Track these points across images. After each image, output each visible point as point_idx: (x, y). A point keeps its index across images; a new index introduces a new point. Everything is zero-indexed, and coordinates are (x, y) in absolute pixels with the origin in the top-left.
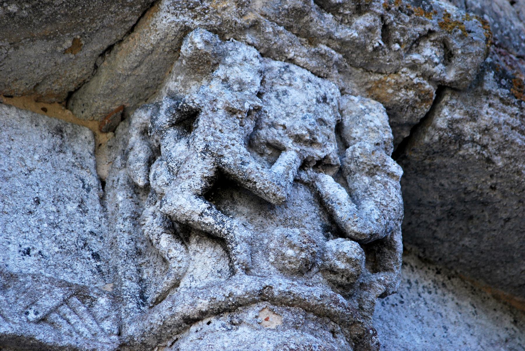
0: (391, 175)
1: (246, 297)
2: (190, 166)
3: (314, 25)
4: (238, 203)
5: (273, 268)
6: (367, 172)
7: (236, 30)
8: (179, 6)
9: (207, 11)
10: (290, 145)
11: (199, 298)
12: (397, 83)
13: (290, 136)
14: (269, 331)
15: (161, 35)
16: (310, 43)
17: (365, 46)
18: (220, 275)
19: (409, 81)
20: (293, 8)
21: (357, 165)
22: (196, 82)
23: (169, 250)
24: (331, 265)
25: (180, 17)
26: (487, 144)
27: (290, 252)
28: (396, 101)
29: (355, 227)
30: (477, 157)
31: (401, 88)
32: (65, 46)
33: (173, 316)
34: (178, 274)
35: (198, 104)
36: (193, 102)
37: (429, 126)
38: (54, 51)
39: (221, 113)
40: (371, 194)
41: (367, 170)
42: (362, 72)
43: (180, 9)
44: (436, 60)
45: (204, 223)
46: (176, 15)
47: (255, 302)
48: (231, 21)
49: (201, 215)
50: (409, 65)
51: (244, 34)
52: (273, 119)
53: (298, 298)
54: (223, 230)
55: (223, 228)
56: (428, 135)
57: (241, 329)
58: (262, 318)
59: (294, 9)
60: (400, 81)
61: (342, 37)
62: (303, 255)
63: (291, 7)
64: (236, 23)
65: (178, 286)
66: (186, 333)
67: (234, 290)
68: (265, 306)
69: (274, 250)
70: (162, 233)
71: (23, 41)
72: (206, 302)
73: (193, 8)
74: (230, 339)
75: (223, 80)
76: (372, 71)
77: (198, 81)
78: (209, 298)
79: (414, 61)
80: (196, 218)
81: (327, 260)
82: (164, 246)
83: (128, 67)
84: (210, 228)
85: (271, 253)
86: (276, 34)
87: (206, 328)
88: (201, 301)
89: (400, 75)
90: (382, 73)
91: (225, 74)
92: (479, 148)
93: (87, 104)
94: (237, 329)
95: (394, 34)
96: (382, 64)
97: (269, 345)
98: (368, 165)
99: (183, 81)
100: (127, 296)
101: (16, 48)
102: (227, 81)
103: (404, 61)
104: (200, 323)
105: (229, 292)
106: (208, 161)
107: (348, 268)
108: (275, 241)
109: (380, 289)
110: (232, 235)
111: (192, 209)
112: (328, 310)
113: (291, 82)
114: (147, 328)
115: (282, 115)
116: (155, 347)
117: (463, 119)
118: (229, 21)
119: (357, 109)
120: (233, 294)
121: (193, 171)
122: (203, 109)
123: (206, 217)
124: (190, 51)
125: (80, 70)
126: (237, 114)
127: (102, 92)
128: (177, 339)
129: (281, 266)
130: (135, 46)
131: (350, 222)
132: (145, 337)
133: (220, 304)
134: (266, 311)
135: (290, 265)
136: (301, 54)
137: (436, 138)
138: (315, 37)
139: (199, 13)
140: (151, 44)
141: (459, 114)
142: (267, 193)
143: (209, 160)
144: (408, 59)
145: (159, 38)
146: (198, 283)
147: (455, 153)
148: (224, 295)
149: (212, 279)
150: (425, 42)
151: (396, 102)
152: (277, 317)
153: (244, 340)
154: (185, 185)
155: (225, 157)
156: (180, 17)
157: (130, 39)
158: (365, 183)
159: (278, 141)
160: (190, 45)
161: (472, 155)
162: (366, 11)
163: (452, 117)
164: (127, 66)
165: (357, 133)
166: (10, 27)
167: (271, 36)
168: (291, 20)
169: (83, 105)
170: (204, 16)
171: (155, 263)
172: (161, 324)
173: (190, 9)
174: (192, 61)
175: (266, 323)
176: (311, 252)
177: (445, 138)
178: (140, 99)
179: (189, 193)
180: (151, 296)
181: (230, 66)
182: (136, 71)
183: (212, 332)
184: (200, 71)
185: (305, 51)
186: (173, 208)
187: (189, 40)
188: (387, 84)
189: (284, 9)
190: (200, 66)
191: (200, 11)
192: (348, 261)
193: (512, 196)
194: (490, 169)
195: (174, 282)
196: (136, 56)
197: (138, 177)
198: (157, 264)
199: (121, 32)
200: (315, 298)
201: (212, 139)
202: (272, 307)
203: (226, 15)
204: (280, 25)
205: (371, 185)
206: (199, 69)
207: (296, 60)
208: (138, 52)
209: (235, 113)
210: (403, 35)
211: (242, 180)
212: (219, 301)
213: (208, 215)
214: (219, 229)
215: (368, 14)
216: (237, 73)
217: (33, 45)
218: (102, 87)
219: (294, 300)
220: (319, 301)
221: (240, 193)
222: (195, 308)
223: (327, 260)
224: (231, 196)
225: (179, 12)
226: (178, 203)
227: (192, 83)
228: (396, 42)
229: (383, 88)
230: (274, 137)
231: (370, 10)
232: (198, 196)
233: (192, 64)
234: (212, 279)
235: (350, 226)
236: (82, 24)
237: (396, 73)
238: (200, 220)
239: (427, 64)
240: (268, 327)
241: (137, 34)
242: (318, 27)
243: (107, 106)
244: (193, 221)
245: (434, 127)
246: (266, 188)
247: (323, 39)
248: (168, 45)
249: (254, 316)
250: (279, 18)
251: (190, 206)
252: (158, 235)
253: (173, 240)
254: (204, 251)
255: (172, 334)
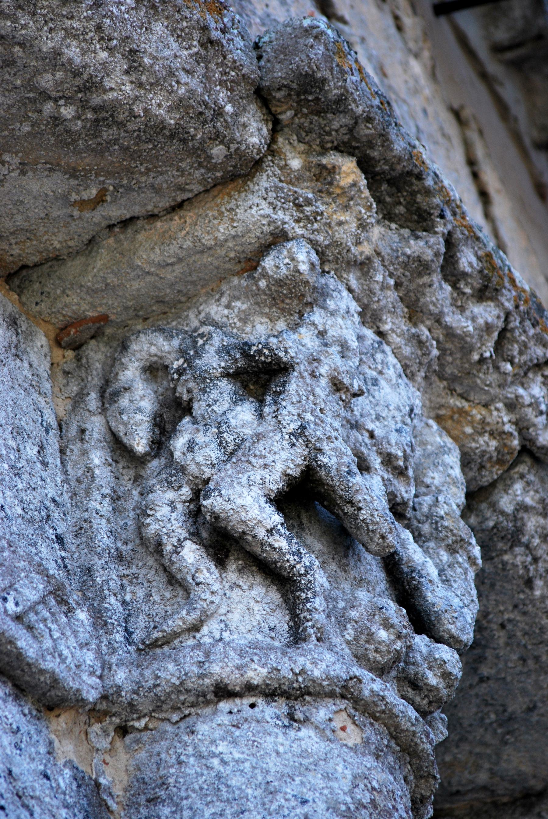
0: (471, 560)
1: (325, 683)
2: (268, 449)
3: (430, 292)
4: (307, 531)
5: (347, 651)
6: (448, 545)
7: (342, 262)
8: (283, 195)
9: (319, 218)
10: (378, 466)
11: (253, 661)
12: (483, 421)
13: (380, 453)
14: (345, 749)
15: (239, 229)
16: (410, 319)
17: (471, 350)
18: (273, 634)
19: (500, 425)
20: (419, 257)
21: (436, 529)
22: (267, 320)
23: (197, 570)
24: (417, 673)
25: (280, 212)
26: (540, 558)
27: (383, 634)
28: (471, 448)
29: (453, 626)
30: (521, 572)
31: (486, 432)
32: (85, 196)
33: (201, 676)
34: (205, 612)
35: (292, 358)
36: (286, 352)
37: (482, 502)
38: (65, 197)
39: (324, 382)
40: (448, 581)
41: (450, 542)
42: (444, 388)
43: (283, 200)
44: (543, 407)
45: (270, 545)
46: (274, 208)
47: (332, 695)
48: (344, 245)
49: (270, 531)
50: (507, 401)
51: (349, 272)
52: (359, 417)
53: (391, 710)
54: (298, 566)
55: (300, 563)
56: (477, 516)
57: (305, 732)
58: (337, 724)
59: (419, 259)
60: (488, 420)
61: (454, 325)
62: (398, 645)
63: (416, 255)
64: (349, 251)
65: (198, 630)
66: (208, 710)
67: (309, 666)
68: (343, 707)
69: (356, 622)
70: (185, 539)
71: (39, 166)
72: (264, 671)
73: (301, 206)
74: (288, 743)
75: (319, 332)
76: (455, 391)
77: (271, 320)
78: (269, 666)
79: (517, 397)
80: (261, 533)
81: (413, 664)
82: (190, 561)
83: (156, 260)
84: (276, 557)
85: (349, 626)
86: (384, 287)
87: (248, 712)
88: (256, 667)
89: (490, 411)
90: (467, 400)
91: (324, 324)
92: (529, 559)
93: (49, 293)
94: (299, 729)
95: (510, 347)
96: (477, 385)
97: (346, 772)
98: (454, 535)
99: (244, 311)
100: (113, 621)
101: (23, 173)
102: (323, 336)
103: (504, 392)
104: (238, 701)
105: (301, 668)
106: (299, 451)
107: (440, 686)
108: (362, 609)
109: (442, 733)
110: (312, 579)
111: (259, 518)
112: (416, 744)
113: (383, 368)
114: (146, 681)
115: (371, 414)
116: (144, 716)
117: (534, 508)
118: (341, 244)
119: (435, 442)
120: (305, 673)
121: (272, 459)
122: (297, 367)
123: (277, 537)
124: (285, 271)
125: (68, 238)
126: (342, 392)
127: (89, 284)
128: (190, 714)
129: (360, 651)
130: (184, 232)
131: (447, 616)
132: (138, 695)
133: (282, 681)
134: (344, 714)
135: (375, 654)
136: (398, 331)
137: (491, 524)
138: (422, 312)
139: (307, 216)
140: (216, 239)
141: (532, 499)
142: (373, 531)
143: (300, 450)
144: (511, 392)
145: (233, 232)
146: (235, 637)
147: (497, 556)
148: (292, 670)
149: (259, 637)
150: (535, 373)
151: (469, 450)
152: (357, 730)
153: (310, 750)
154: (257, 475)
155: (324, 454)
156: (279, 212)
157: (176, 218)
158: (441, 561)
159: (363, 454)
160: (287, 261)
161: (517, 566)
162: (491, 299)
163: (523, 501)
164: (156, 256)
165: (433, 478)
166: (41, 139)
167: (377, 287)
168: (407, 273)
169: (42, 293)
170: (312, 224)
171: (150, 582)
172: (178, 683)
173: (296, 205)
174: (281, 286)
175: (341, 734)
176: (408, 644)
177: (503, 527)
178: (136, 315)
179: (259, 492)
180: (138, 631)
181: (333, 314)
182: (164, 271)
183: (258, 721)
184: (282, 305)
185: (405, 328)
186: (230, 507)
187: (285, 252)
188: (469, 418)
189: (404, 254)
190: (287, 298)
191: (309, 214)
192: (443, 675)
193: (519, 645)
194: (522, 596)
195: (194, 622)
196: (181, 247)
197: (137, 438)
198: (154, 584)
199: (165, 203)
200: (410, 720)
201: (312, 419)
202: (352, 711)
203: (341, 234)
204: (391, 275)
205: (449, 566)
206: (283, 301)
207: (389, 337)
208: (188, 244)
209: (338, 390)
210: (521, 353)
211: (341, 497)
212: (284, 677)
213: (281, 536)
214: (292, 563)
215: (492, 304)
216: (341, 328)
217: (47, 176)
218: (95, 276)
219: (383, 712)
220: (413, 725)
221: (310, 516)
222: (242, 675)
223: (413, 664)
224: (299, 517)
225: (279, 204)
226: (239, 501)
227: (258, 319)
228: (509, 361)
229: (459, 422)
230: (358, 445)
231: (497, 299)
232: (270, 501)
233: (276, 291)
234: (259, 637)
235: (446, 622)
236: (130, 171)
237: (486, 406)
238: (266, 538)
239: (531, 409)
240: (345, 742)
241: (191, 214)
242: (434, 299)
243: (82, 309)
244: (254, 537)
245: (493, 506)
246: (373, 522)
247: (428, 319)
248: (237, 248)
249: (327, 718)
250: (393, 265)
251: (257, 512)
252: (179, 540)
253: (204, 555)
254: (251, 587)
255: (183, 704)
